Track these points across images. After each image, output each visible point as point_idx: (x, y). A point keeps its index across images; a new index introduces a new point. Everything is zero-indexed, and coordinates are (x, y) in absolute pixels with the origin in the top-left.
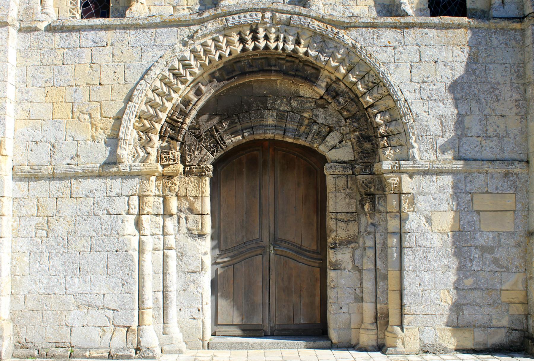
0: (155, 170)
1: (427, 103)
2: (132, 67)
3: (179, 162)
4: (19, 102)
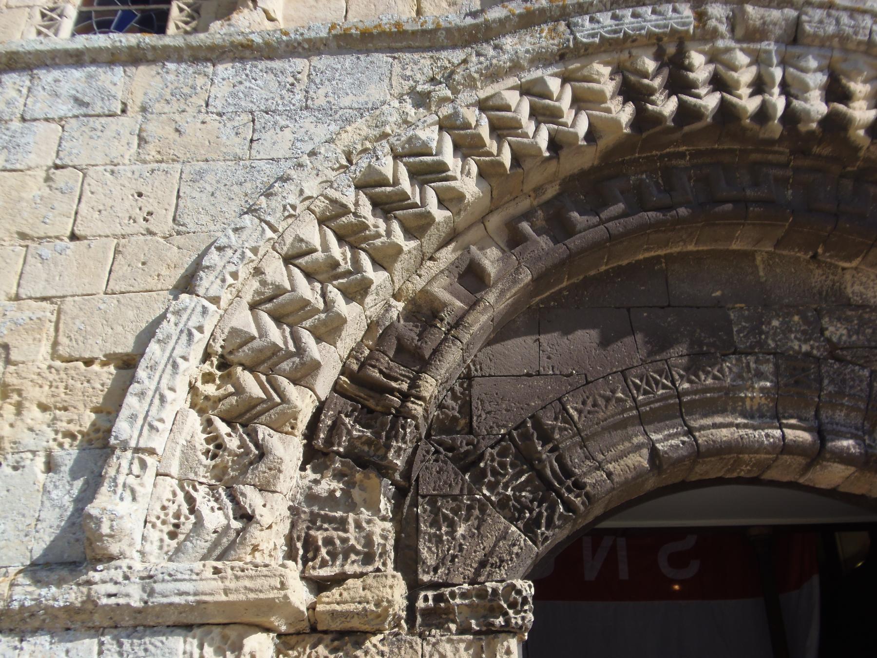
0: (272, 595)
2: (209, 177)
3: (390, 565)
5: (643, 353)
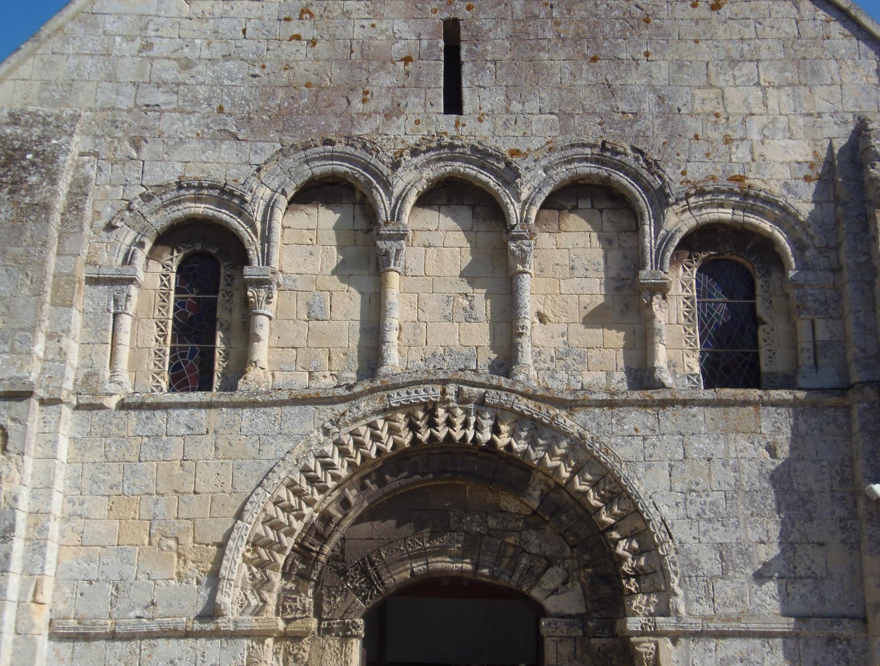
1: (696, 524)
2: (244, 467)
3: (312, 615)
4: (67, 518)
5: (412, 531)
